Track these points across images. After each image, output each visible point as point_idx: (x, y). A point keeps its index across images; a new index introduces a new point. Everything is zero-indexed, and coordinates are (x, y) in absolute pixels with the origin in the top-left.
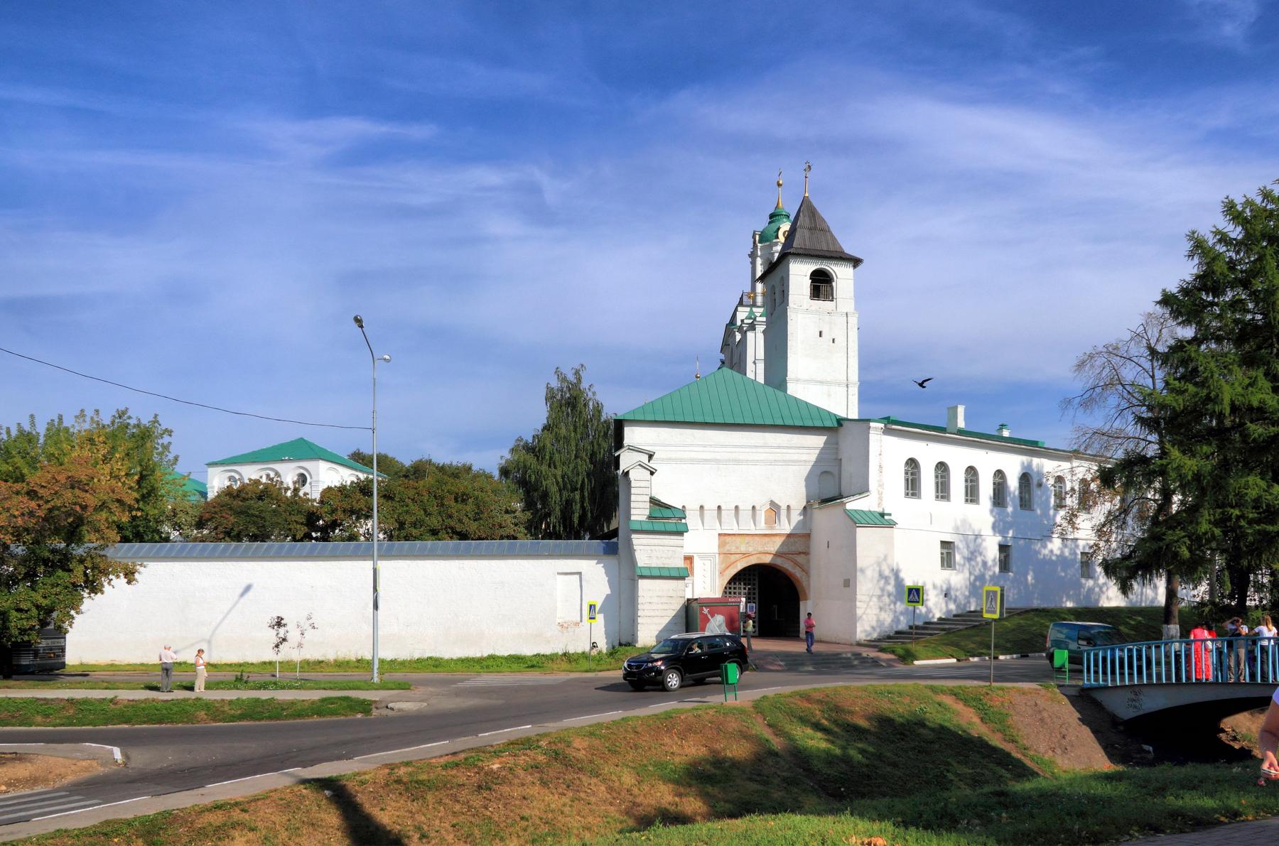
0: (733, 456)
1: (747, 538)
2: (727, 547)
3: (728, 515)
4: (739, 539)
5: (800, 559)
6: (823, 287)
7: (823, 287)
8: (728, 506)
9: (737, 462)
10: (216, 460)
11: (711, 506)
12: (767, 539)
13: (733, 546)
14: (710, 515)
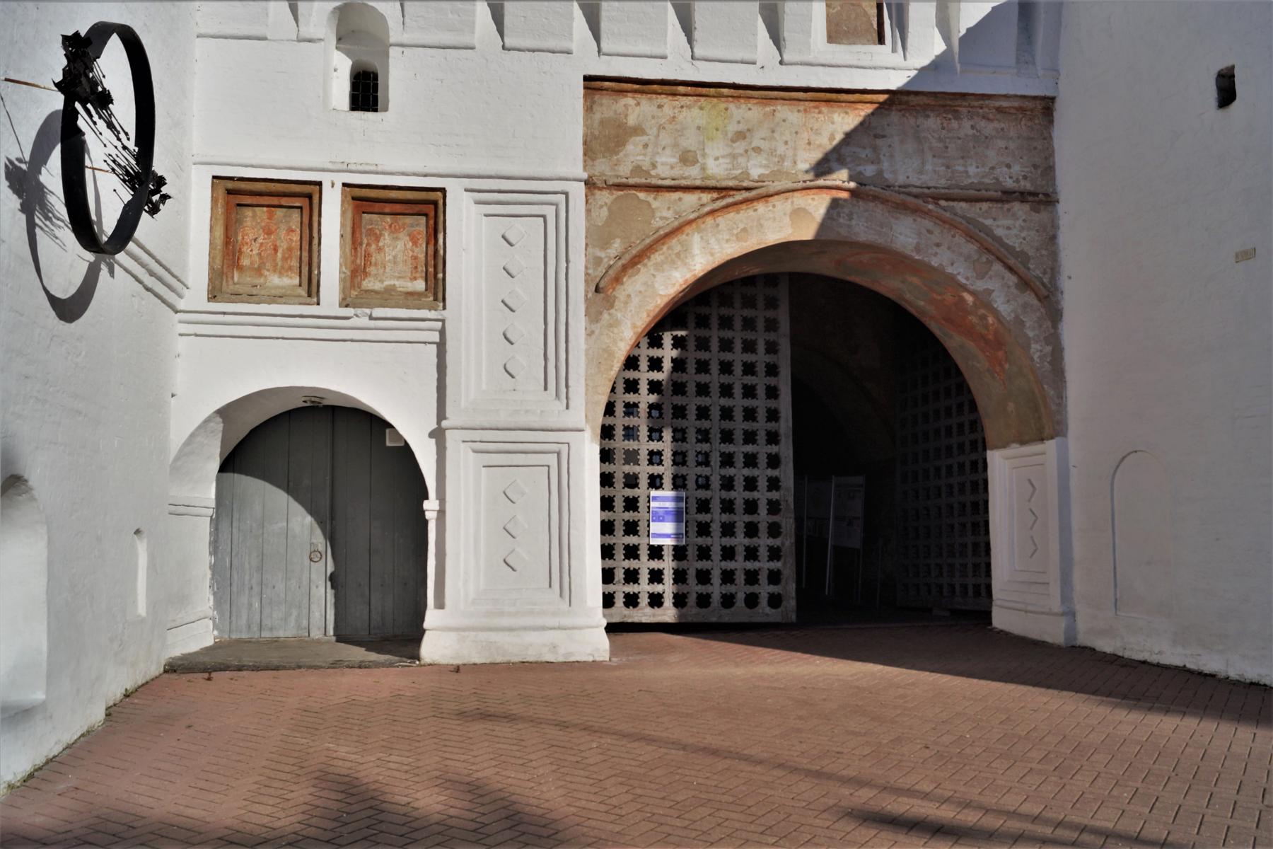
2: (633, 155)
13: (665, 140)
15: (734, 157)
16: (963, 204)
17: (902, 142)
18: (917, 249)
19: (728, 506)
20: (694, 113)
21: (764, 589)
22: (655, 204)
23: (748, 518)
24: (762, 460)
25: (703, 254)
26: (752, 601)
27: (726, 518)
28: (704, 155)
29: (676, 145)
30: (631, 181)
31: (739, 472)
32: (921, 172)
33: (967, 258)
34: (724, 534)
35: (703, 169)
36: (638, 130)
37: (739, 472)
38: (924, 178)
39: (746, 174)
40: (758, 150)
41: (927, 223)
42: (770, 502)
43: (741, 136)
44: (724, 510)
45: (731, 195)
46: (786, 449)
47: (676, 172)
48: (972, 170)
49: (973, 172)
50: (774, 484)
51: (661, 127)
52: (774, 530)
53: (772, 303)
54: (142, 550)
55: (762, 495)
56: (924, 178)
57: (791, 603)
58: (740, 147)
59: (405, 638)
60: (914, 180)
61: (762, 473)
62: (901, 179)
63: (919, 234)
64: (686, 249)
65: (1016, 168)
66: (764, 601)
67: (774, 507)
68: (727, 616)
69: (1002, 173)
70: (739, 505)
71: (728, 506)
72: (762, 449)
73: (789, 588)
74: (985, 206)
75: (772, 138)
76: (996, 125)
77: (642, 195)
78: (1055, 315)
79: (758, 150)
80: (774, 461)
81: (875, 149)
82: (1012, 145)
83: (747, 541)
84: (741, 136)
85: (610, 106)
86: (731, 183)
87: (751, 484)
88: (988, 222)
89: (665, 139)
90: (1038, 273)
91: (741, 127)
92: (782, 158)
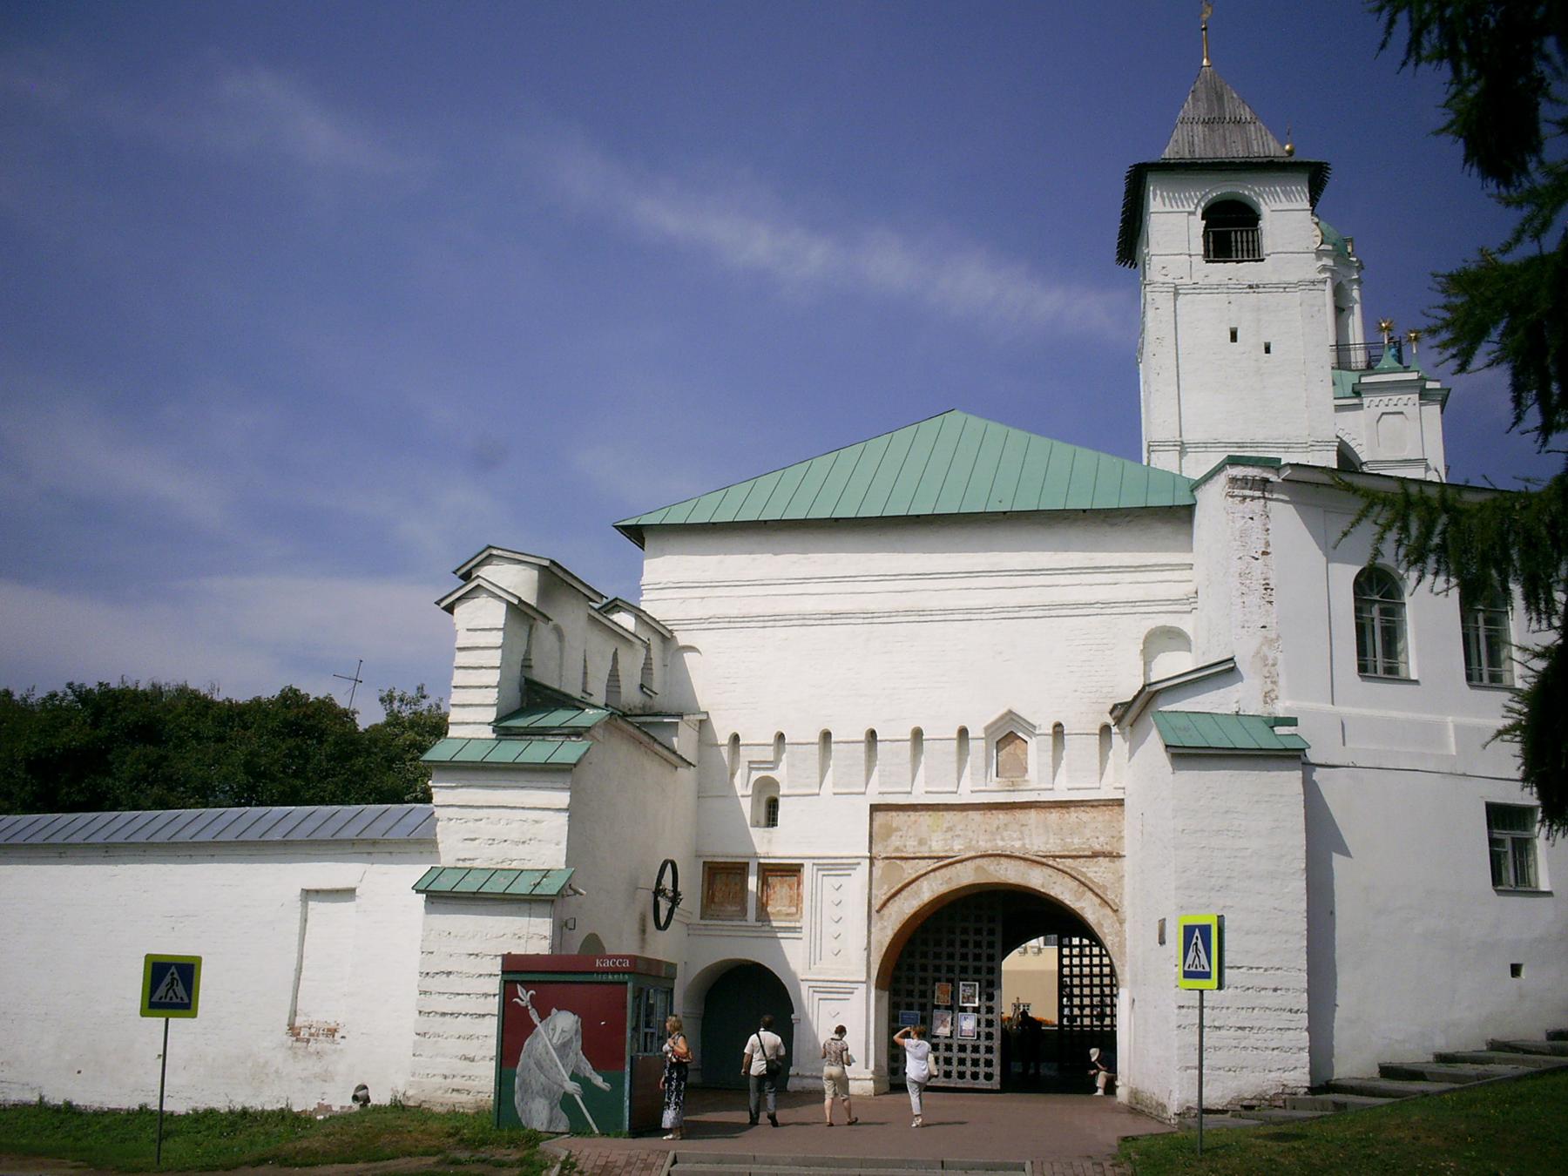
0: (908, 601)
1: (1054, 816)
2: (895, 841)
3: (893, 754)
4: (925, 818)
5: (1096, 872)
6: (1237, 236)
7: (1237, 236)
8: (893, 731)
9: (922, 615)
10: (589, 679)
11: (848, 731)
12: (1002, 817)
13: (912, 835)
14: (847, 756)
17: (1454, 356)
21: (982, 1070)
25: (928, 891)
26: (975, 1076)
36: (898, 829)
39: (952, 849)
43: (950, 829)
45: (946, 862)
48: (1076, 841)
50: (989, 1063)
53: (991, 932)
54: (676, 1046)
57: (997, 1078)
58: (949, 835)
65: (1101, 839)
66: (981, 1076)
68: (961, 1084)
73: (996, 1070)
84: (950, 829)
85: (880, 817)
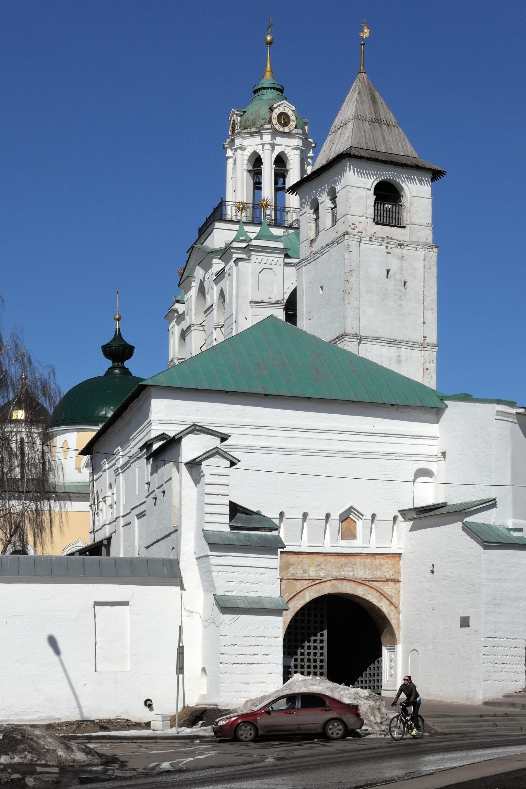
2: (291, 570)
15: (316, 571)
16: (376, 583)
18: (363, 595)
19: (309, 660)
20: (306, 559)
22: (297, 584)
23: (314, 664)
24: (319, 648)
27: (308, 664)
28: (309, 571)
29: (302, 568)
30: (291, 578)
31: (312, 651)
32: (365, 574)
33: (376, 597)
34: (308, 668)
35: (309, 574)
36: (293, 564)
37: (312, 651)
38: (366, 575)
39: (320, 575)
40: (323, 569)
41: (366, 588)
42: (320, 660)
43: (318, 565)
44: (308, 662)
45: (317, 581)
46: (325, 644)
47: (302, 575)
48: (379, 573)
49: (379, 574)
50: (322, 641)
51: (298, 563)
52: (321, 667)
55: (318, 658)
56: (366, 575)
58: (318, 568)
59: (109, 556)
60: (363, 576)
61: (319, 651)
62: (360, 576)
63: (364, 591)
64: (304, 596)
65: (390, 573)
67: (322, 661)
69: (386, 574)
70: (312, 660)
71: (309, 660)
72: (319, 645)
74: (381, 583)
75: (326, 566)
76: (385, 561)
77: (293, 581)
78: (399, 613)
79: (323, 569)
80: (322, 648)
81: (353, 568)
82: (390, 566)
83: (314, 670)
84: (318, 565)
86: (316, 578)
87: (315, 654)
88: (382, 587)
89: (299, 567)
90: (395, 601)
91: (319, 563)
92: (329, 571)
